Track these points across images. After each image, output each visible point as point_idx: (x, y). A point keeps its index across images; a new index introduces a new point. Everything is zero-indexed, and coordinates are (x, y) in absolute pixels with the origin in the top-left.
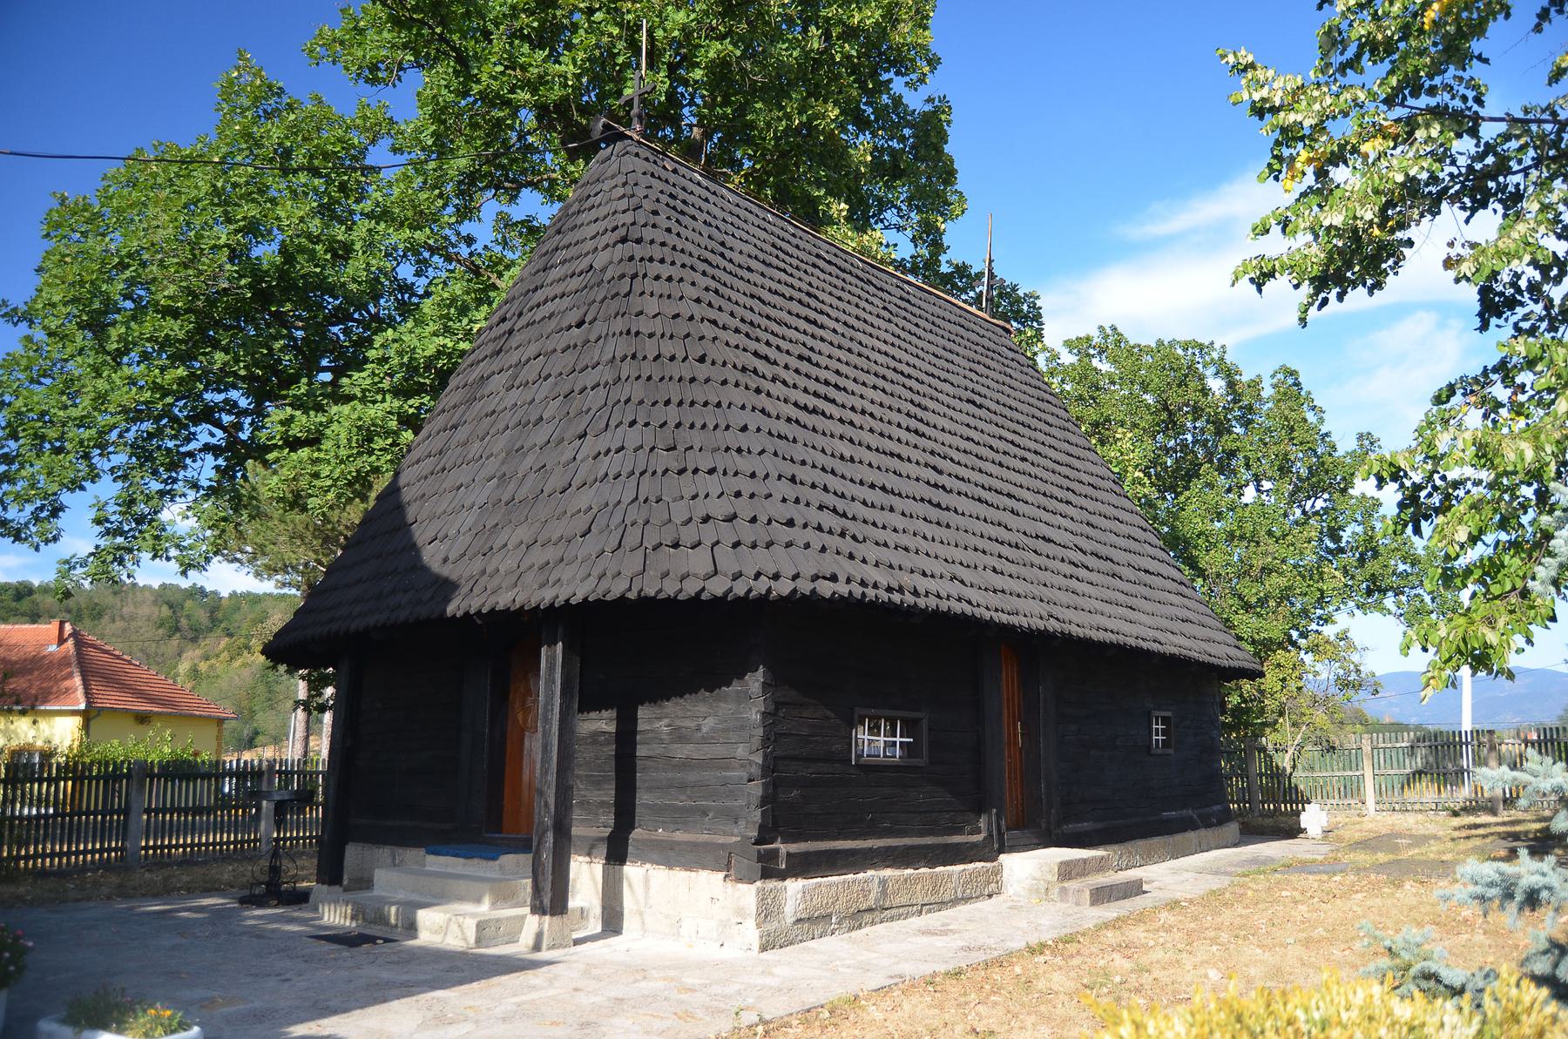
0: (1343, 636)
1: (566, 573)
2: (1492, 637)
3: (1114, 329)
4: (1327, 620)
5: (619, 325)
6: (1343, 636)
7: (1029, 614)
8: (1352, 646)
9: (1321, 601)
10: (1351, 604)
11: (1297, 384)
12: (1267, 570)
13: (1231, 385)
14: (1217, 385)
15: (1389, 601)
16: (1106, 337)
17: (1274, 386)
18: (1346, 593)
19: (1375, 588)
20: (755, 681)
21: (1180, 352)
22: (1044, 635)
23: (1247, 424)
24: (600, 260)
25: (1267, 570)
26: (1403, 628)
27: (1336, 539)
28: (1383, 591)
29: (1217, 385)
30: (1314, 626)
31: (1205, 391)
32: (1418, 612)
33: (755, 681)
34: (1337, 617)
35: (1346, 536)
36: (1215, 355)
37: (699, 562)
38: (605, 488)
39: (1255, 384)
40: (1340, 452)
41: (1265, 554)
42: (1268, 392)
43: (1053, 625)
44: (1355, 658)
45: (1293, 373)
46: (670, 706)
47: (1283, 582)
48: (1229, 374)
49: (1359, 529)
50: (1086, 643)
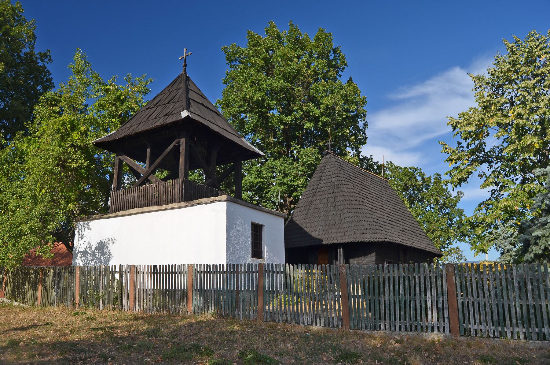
0: (458, 248)
1: (347, 237)
2: (485, 248)
3: (391, 162)
4: (450, 244)
5: (341, 194)
6: (458, 248)
7: (408, 244)
8: (459, 250)
9: (448, 239)
10: (456, 240)
11: (440, 177)
12: (434, 231)
13: (423, 179)
14: (419, 178)
15: (467, 239)
16: (389, 164)
17: (434, 179)
18: (455, 236)
19: (463, 235)
20: (373, 254)
21: (410, 170)
22: (411, 247)
23: (427, 189)
24: (333, 180)
25: (434, 231)
26: (470, 246)
27: (451, 221)
28: (465, 236)
29: (419, 178)
30: (446, 246)
31: (416, 181)
32: (474, 242)
33: (373, 254)
34: (453, 243)
35: (455, 220)
36: (419, 171)
37: (368, 236)
38: (348, 223)
39: (430, 178)
40: (453, 197)
41: (434, 226)
42: (433, 181)
43: (412, 246)
44: (461, 253)
45: (439, 175)
46: (357, 259)
47: (439, 233)
48: (422, 175)
49: (458, 219)
50: (416, 249)
